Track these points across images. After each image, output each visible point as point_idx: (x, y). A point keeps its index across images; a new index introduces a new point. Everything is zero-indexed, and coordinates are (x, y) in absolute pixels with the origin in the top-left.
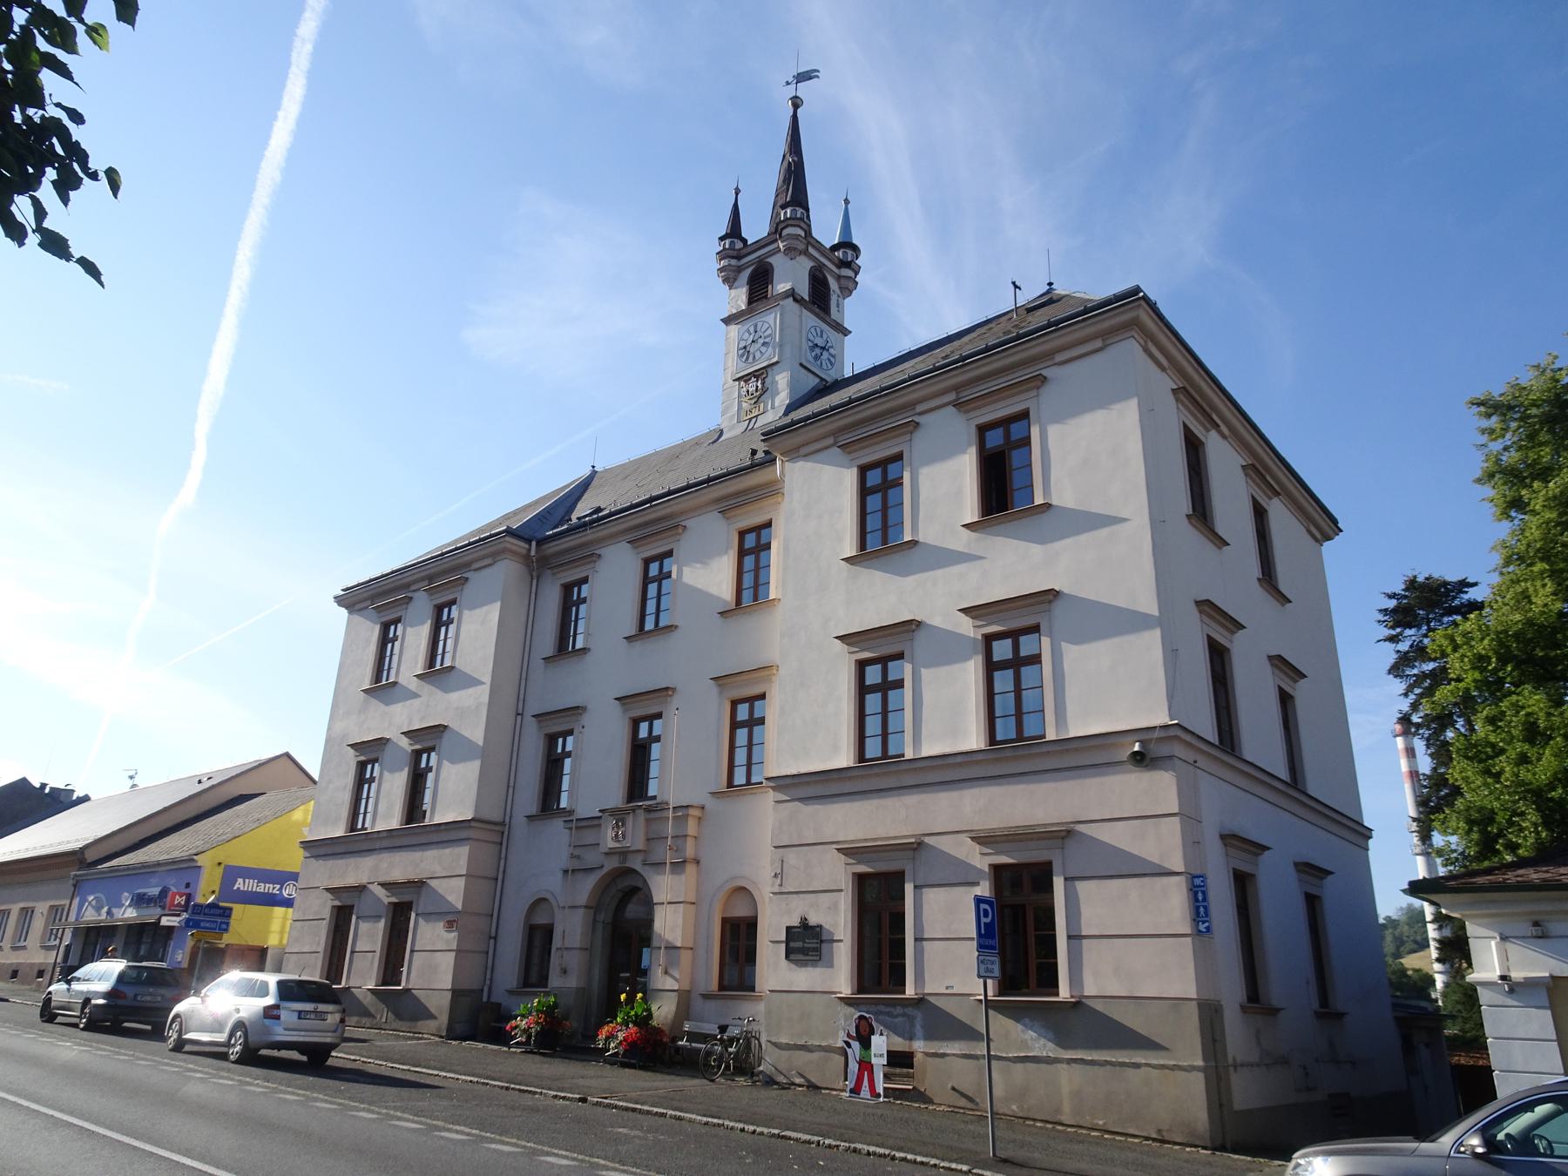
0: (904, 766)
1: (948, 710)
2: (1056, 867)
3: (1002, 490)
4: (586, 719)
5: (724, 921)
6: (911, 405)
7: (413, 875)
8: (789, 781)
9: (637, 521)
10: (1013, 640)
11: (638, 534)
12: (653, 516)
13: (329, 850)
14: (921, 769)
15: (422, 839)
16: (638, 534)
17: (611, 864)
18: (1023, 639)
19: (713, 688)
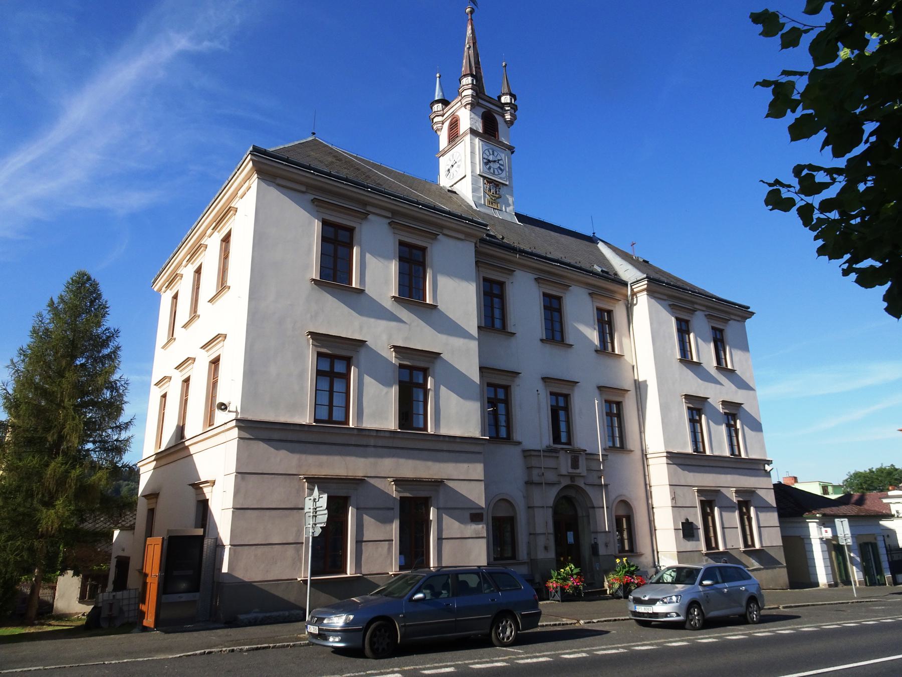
0: (346, 432)
1: (376, 406)
2: (353, 500)
3: (411, 290)
4: (518, 381)
5: (616, 516)
6: (442, 227)
7: (360, 474)
8: (298, 428)
9: (296, 177)
10: (414, 375)
11: (543, 276)
12: (557, 272)
13: (290, 436)
14: (275, 429)
15: (706, 463)
16: (543, 276)
17: (566, 482)
18: (336, 361)
19: (540, 385)
